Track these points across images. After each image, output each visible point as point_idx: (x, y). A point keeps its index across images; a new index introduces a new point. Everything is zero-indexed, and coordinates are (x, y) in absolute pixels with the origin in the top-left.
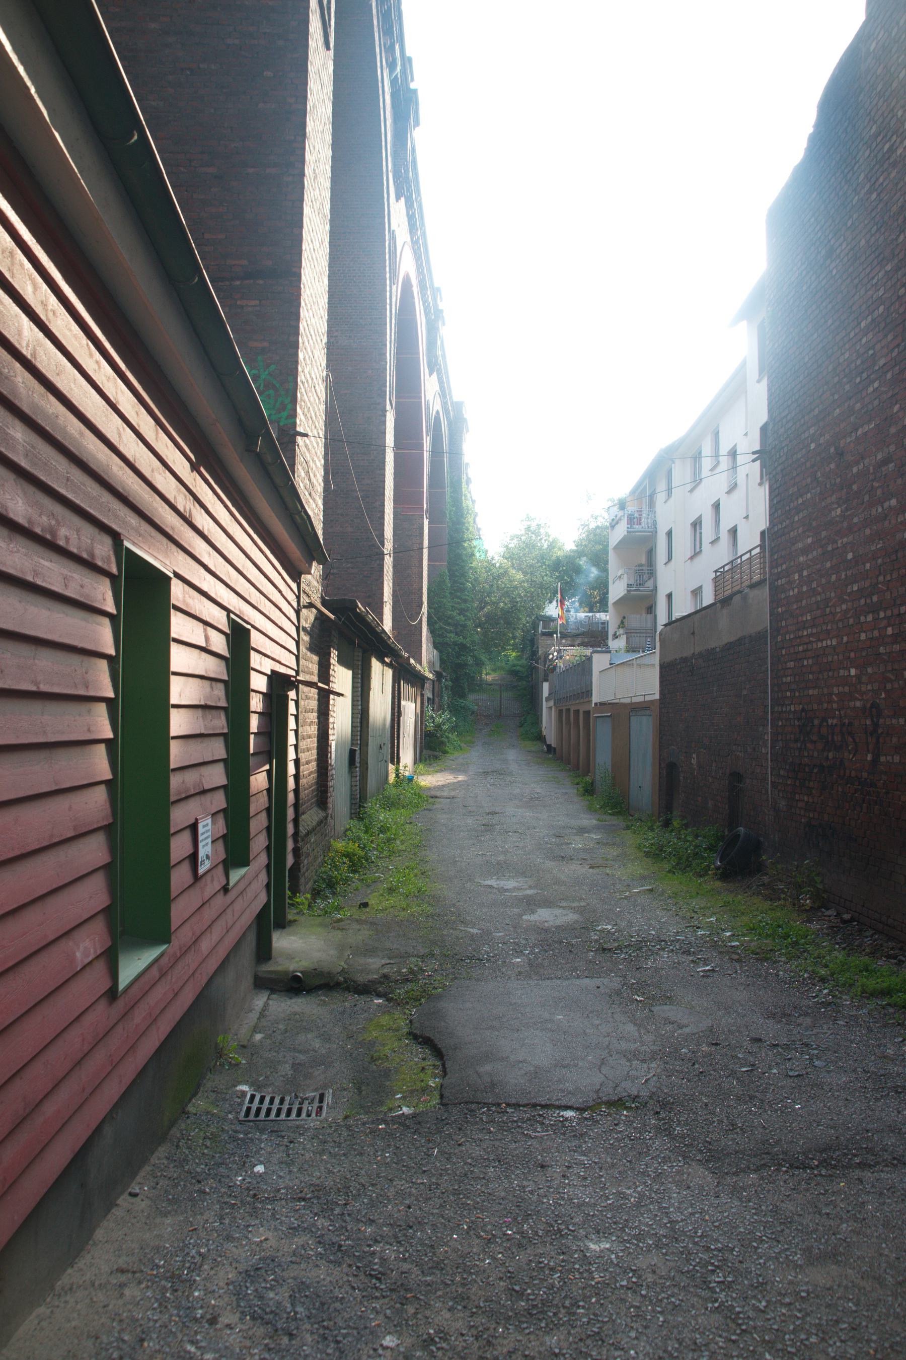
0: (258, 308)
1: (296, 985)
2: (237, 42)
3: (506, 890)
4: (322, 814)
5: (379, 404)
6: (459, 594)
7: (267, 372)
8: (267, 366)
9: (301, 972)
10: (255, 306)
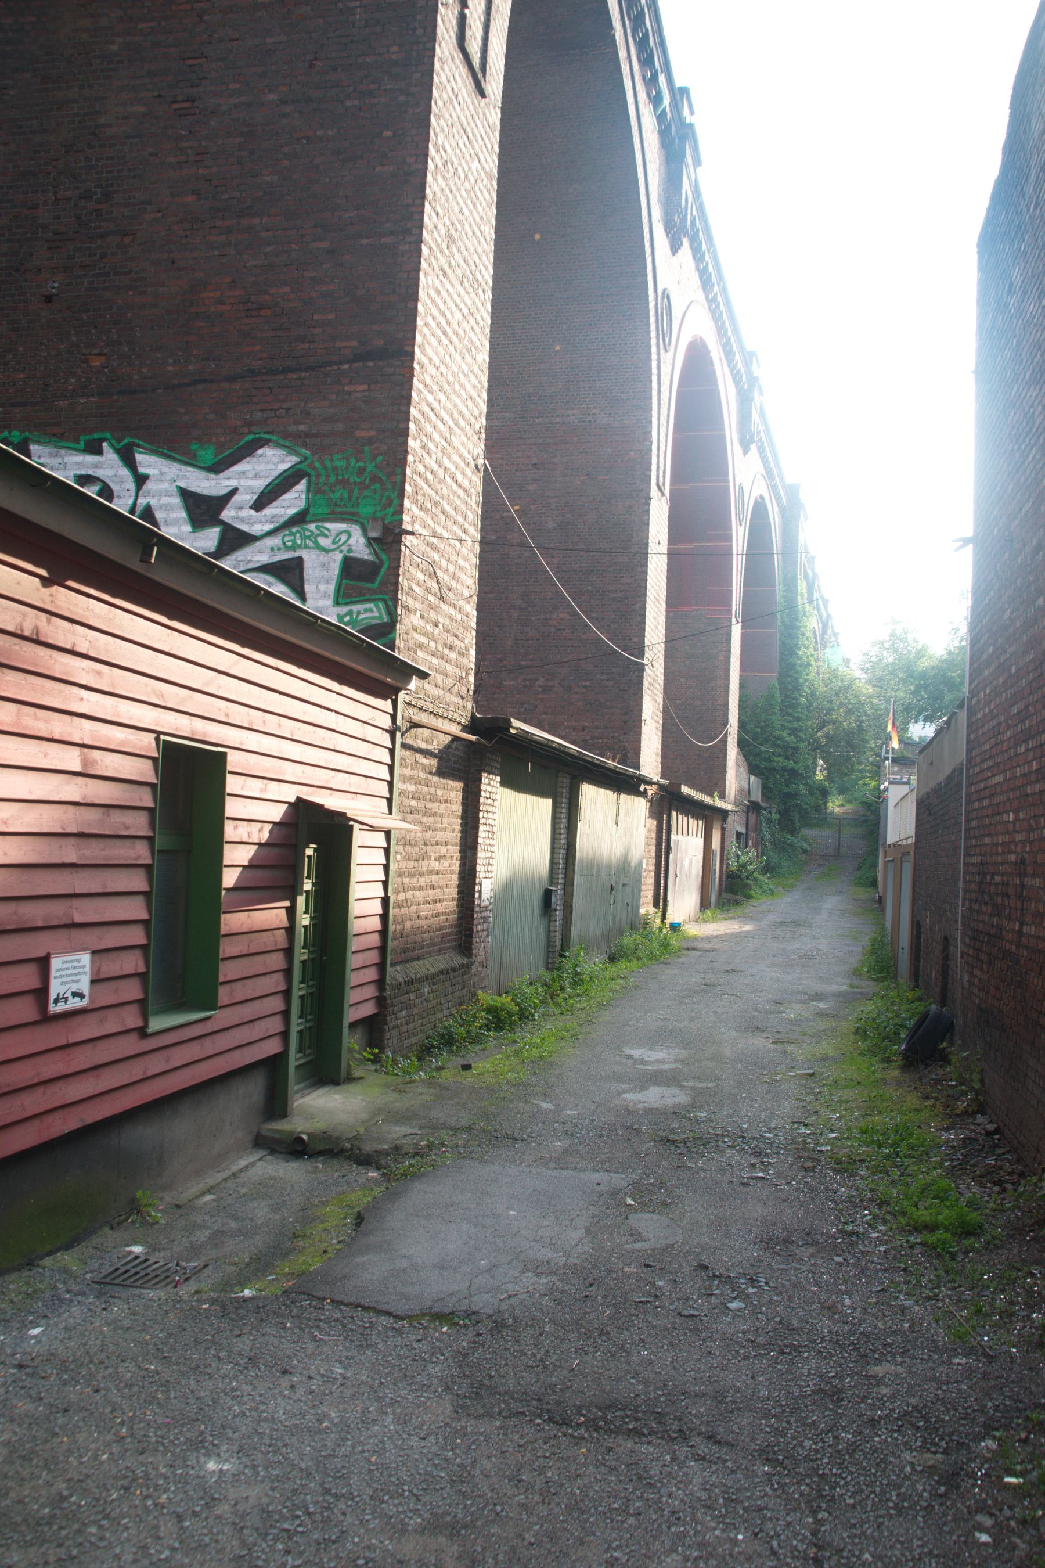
0: (366, 394)
1: (299, 1148)
2: (356, 102)
3: (645, 1063)
4: (458, 960)
5: (641, 491)
6: (790, 711)
7: (373, 464)
8: (374, 457)
9: (308, 1134)
10: (363, 391)
